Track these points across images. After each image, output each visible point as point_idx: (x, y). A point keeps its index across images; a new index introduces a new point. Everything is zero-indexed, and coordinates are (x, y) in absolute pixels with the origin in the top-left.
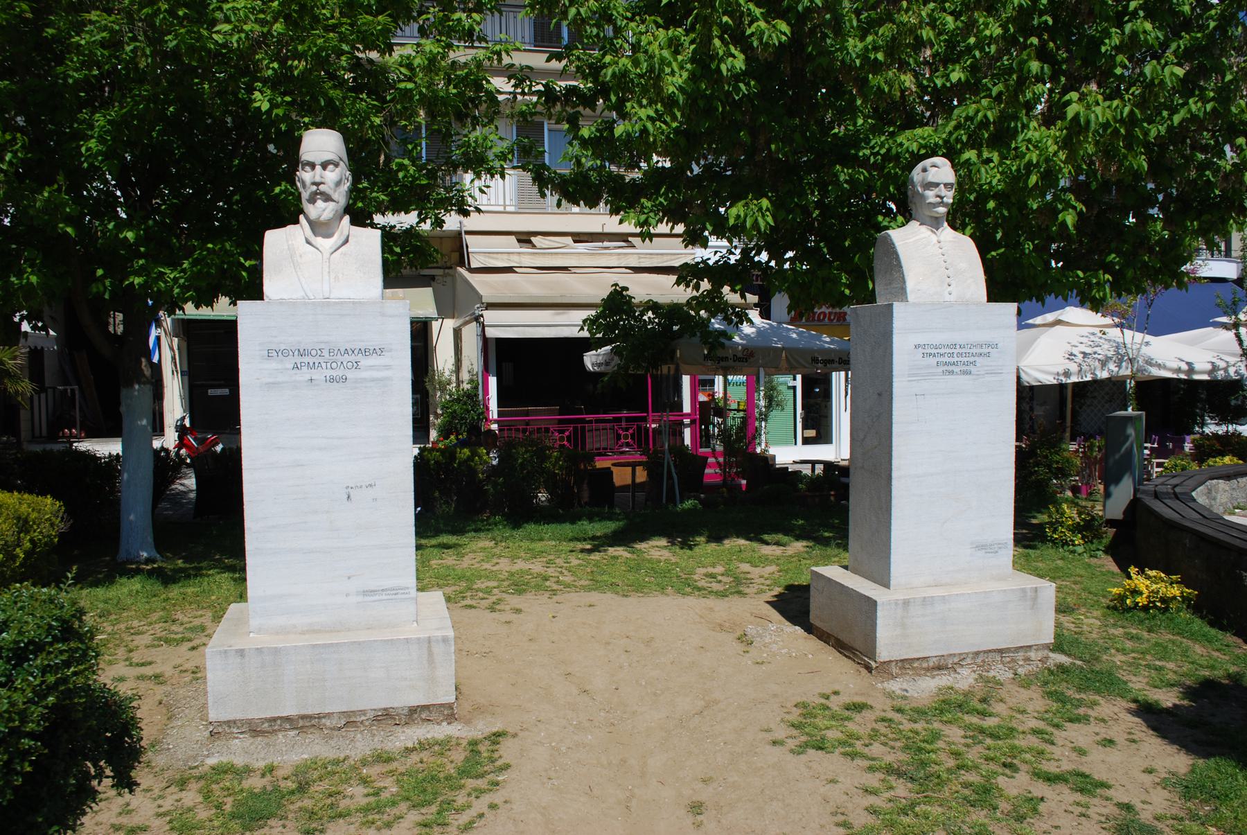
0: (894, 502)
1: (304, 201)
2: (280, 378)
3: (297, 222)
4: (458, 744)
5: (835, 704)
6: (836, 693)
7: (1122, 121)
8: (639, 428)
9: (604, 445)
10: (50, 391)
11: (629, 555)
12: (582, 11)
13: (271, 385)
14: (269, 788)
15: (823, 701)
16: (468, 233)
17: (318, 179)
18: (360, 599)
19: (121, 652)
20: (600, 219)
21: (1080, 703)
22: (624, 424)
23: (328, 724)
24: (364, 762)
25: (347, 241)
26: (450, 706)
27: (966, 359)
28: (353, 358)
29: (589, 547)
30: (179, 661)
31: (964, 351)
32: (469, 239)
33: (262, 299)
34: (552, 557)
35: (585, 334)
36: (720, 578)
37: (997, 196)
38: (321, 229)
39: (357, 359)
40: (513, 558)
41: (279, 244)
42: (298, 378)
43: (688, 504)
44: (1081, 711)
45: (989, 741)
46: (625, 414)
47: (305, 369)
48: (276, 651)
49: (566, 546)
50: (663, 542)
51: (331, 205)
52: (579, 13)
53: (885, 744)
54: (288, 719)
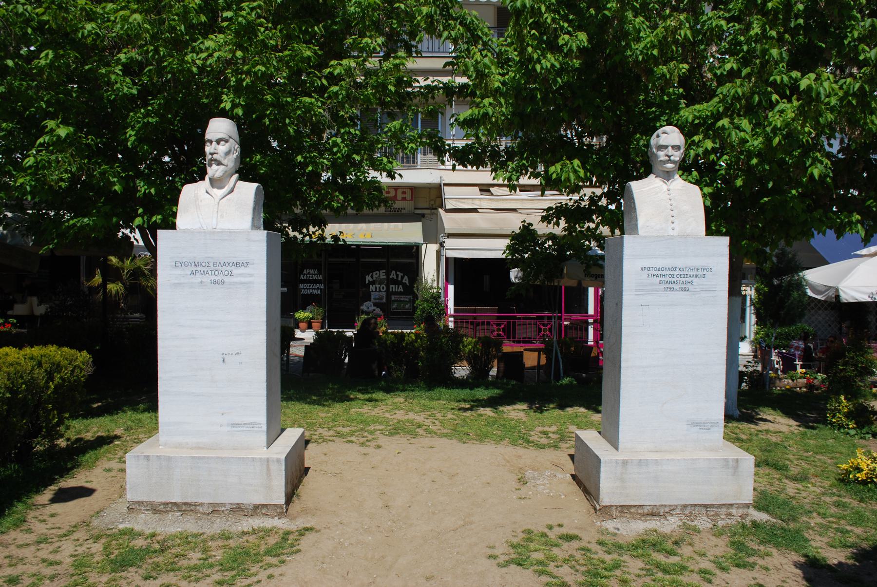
0: (622, 386)
4: (276, 533)
5: (552, 535)
6: (560, 526)
7: (854, 95)
9: (529, 335)
14: (144, 547)
15: (546, 530)
18: (229, 428)
20: (484, 176)
21: (754, 553)
22: (545, 321)
23: (201, 510)
24: (213, 538)
27: (684, 279)
28: (229, 268)
31: (682, 273)
33: (175, 229)
34: (435, 412)
36: (550, 435)
37: (759, 155)
39: (231, 269)
41: (191, 193)
43: (566, 381)
44: (751, 560)
45: (660, 575)
47: (198, 275)
48: (169, 459)
49: (454, 404)
50: (524, 406)
51: (222, 167)
53: (572, 567)
54: (175, 504)
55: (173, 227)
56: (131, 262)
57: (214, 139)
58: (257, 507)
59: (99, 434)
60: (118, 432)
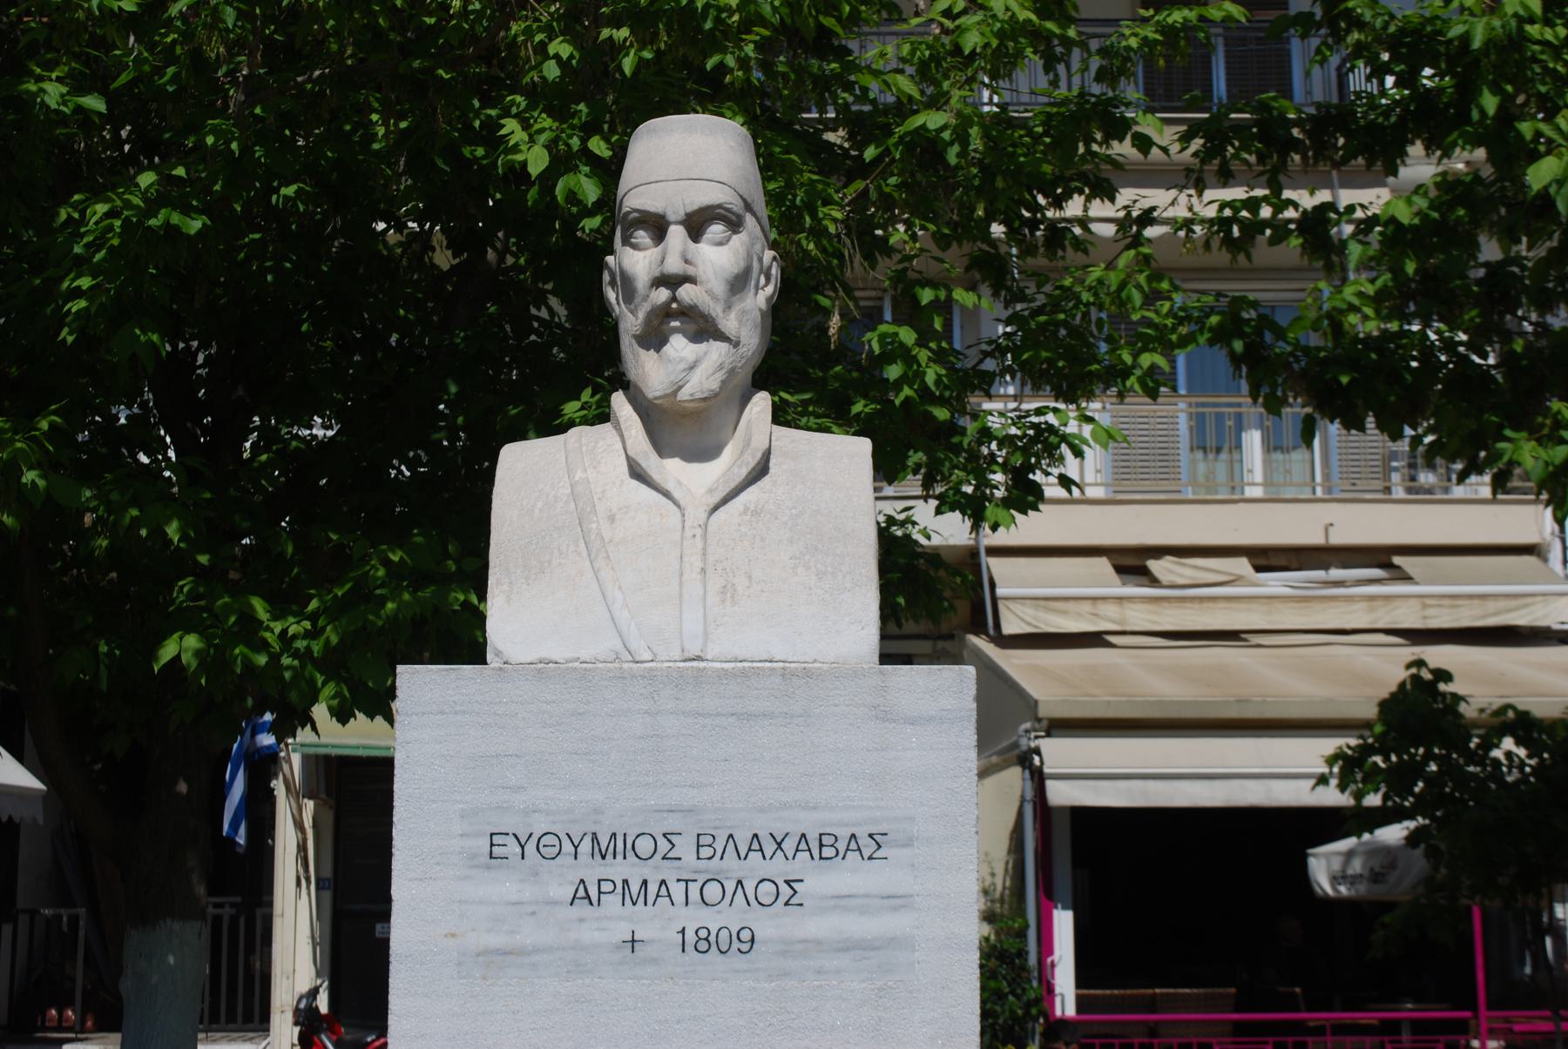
1: (628, 345)
2: (529, 935)
3: (602, 415)
10: (23, 920)
13: (495, 959)
16: (995, 551)
17: (674, 265)
25: (761, 470)
28: (778, 867)
32: (996, 566)
35: (1331, 796)
38: (680, 429)
42: (589, 934)
46: (1408, 1010)
47: (612, 902)
51: (715, 352)
55: (461, 641)
57: (675, 211)
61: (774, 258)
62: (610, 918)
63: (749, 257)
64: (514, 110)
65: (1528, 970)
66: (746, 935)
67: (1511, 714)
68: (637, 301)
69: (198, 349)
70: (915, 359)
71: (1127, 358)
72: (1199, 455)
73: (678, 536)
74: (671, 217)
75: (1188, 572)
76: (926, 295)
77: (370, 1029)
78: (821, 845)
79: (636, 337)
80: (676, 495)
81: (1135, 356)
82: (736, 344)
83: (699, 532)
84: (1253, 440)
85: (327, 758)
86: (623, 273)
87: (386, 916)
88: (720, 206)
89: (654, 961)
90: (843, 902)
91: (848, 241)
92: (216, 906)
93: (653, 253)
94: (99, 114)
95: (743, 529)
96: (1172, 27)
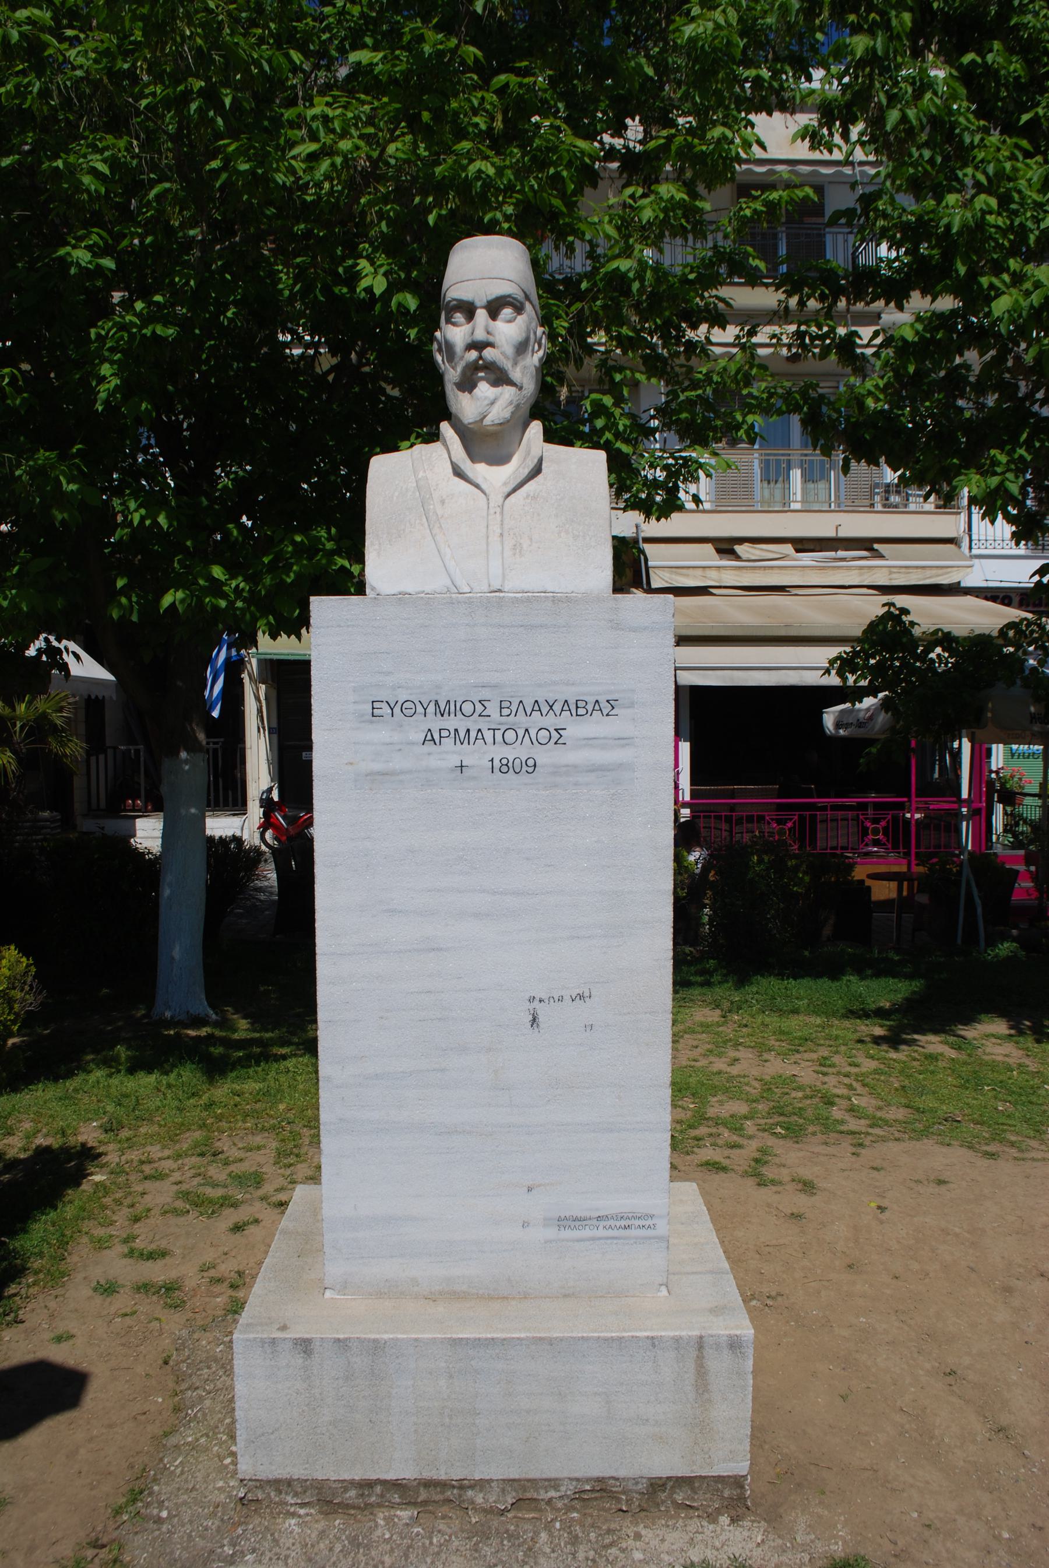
1: (450, 390)
2: (398, 763)
8: (895, 819)
9: (843, 842)
11: (953, 1054)
12: (911, 113)
17: (480, 335)
18: (551, 1233)
19: (121, 1217)
23: (479, 1499)
25: (537, 471)
26: (737, 1482)
28: (551, 721)
29: (878, 1031)
30: (209, 1256)
32: (648, 548)
35: (834, 680)
38: (485, 444)
39: (560, 722)
40: (761, 1048)
42: (434, 762)
43: (1005, 948)
46: (873, 797)
47: (448, 742)
48: (376, 1347)
51: (507, 393)
52: (904, 119)
55: (352, 584)
56: (27, 708)
57: (481, 300)
58: (657, 1486)
59: (40, 1141)
60: (89, 1134)
61: (544, 333)
62: (447, 753)
63: (528, 331)
64: (365, 253)
65: (936, 775)
66: (531, 762)
67: (940, 634)
68: (456, 360)
69: (183, 420)
70: (612, 414)
71: (739, 418)
72: (765, 485)
73: (485, 514)
74: (478, 303)
75: (757, 552)
76: (618, 377)
77: (301, 810)
78: (577, 707)
79: (456, 384)
80: (483, 486)
81: (744, 416)
82: (521, 388)
83: (498, 510)
84: (796, 475)
85: (271, 660)
86: (447, 342)
87: (309, 748)
88: (509, 296)
89: (474, 778)
90: (590, 742)
91: (572, 342)
92: (214, 743)
93: (466, 328)
94: (111, 270)
95: (526, 508)
96: (772, 202)
